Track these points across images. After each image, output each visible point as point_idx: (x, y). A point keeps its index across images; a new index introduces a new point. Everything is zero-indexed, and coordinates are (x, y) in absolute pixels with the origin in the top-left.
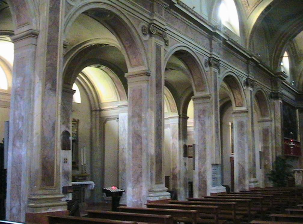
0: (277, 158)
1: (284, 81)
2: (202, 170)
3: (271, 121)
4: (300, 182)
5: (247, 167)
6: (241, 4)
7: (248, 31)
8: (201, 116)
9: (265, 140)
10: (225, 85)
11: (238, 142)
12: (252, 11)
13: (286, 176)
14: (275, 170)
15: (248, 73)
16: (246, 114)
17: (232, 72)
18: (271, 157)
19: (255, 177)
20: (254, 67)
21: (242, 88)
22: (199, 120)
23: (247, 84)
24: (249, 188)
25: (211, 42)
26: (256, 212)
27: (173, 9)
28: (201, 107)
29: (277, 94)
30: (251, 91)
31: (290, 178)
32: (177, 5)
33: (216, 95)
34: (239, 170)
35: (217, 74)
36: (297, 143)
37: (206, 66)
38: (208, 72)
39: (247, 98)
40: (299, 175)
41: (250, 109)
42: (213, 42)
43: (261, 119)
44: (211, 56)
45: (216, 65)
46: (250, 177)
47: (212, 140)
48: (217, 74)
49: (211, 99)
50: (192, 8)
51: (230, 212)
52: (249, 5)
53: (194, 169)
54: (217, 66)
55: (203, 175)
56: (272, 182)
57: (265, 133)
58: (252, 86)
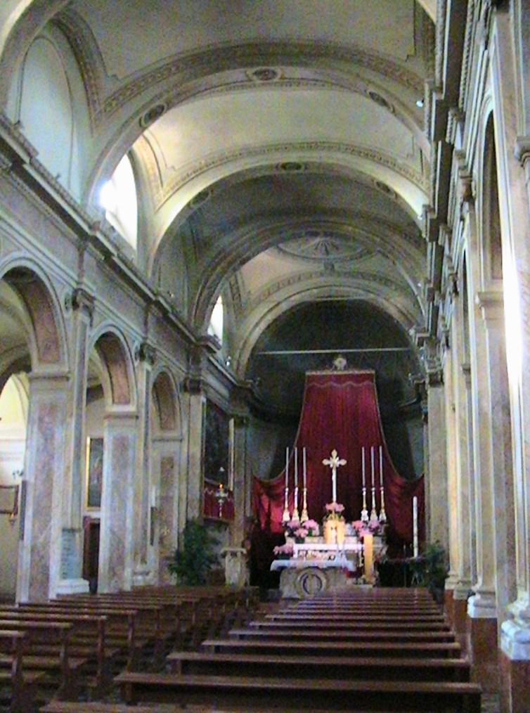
0: (189, 523)
1: (213, 357)
2: (41, 539)
3: (181, 441)
4: (236, 575)
5: (129, 540)
6: (146, 180)
7: (154, 242)
8: (47, 419)
9: (165, 482)
10: (96, 355)
11: (113, 482)
12: (167, 197)
13: (207, 563)
14: (183, 549)
15: (146, 331)
16: (133, 421)
17: (114, 326)
18: (177, 523)
19: (146, 563)
20: (158, 319)
21: (131, 364)
22: (40, 428)
23: (141, 355)
24: (133, 587)
25: (81, 255)
26: (83, 661)
27: (17, 173)
28: (47, 398)
29: (199, 382)
30: (148, 373)
31: (213, 567)
32: (27, 167)
33: (81, 375)
34: (112, 545)
35: (88, 328)
36: (231, 494)
37: (67, 308)
38: (71, 321)
39: (139, 385)
40: (235, 562)
41: (143, 411)
42: (86, 256)
43: (158, 434)
44: (79, 287)
45: (86, 307)
46: (135, 560)
47: (66, 474)
48: (88, 328)
49: (71, 381)
50: (54, 175)
51: (54, 649)
52: (162, 186)
53: (23, 539)
54: (90, 312)
55: (42, 553)
56: (175, 575)
57: (167, 465)
58: (152, 362)
